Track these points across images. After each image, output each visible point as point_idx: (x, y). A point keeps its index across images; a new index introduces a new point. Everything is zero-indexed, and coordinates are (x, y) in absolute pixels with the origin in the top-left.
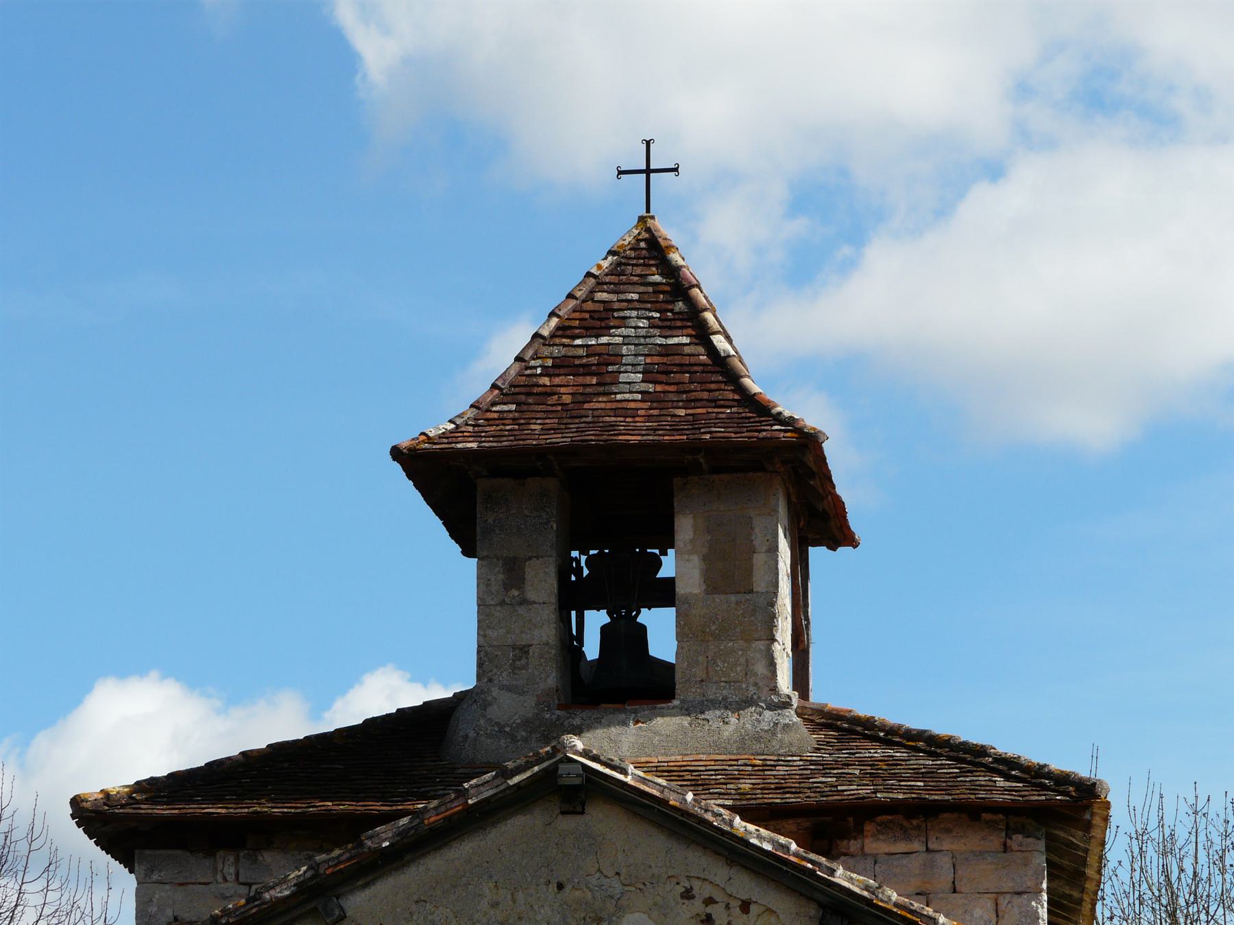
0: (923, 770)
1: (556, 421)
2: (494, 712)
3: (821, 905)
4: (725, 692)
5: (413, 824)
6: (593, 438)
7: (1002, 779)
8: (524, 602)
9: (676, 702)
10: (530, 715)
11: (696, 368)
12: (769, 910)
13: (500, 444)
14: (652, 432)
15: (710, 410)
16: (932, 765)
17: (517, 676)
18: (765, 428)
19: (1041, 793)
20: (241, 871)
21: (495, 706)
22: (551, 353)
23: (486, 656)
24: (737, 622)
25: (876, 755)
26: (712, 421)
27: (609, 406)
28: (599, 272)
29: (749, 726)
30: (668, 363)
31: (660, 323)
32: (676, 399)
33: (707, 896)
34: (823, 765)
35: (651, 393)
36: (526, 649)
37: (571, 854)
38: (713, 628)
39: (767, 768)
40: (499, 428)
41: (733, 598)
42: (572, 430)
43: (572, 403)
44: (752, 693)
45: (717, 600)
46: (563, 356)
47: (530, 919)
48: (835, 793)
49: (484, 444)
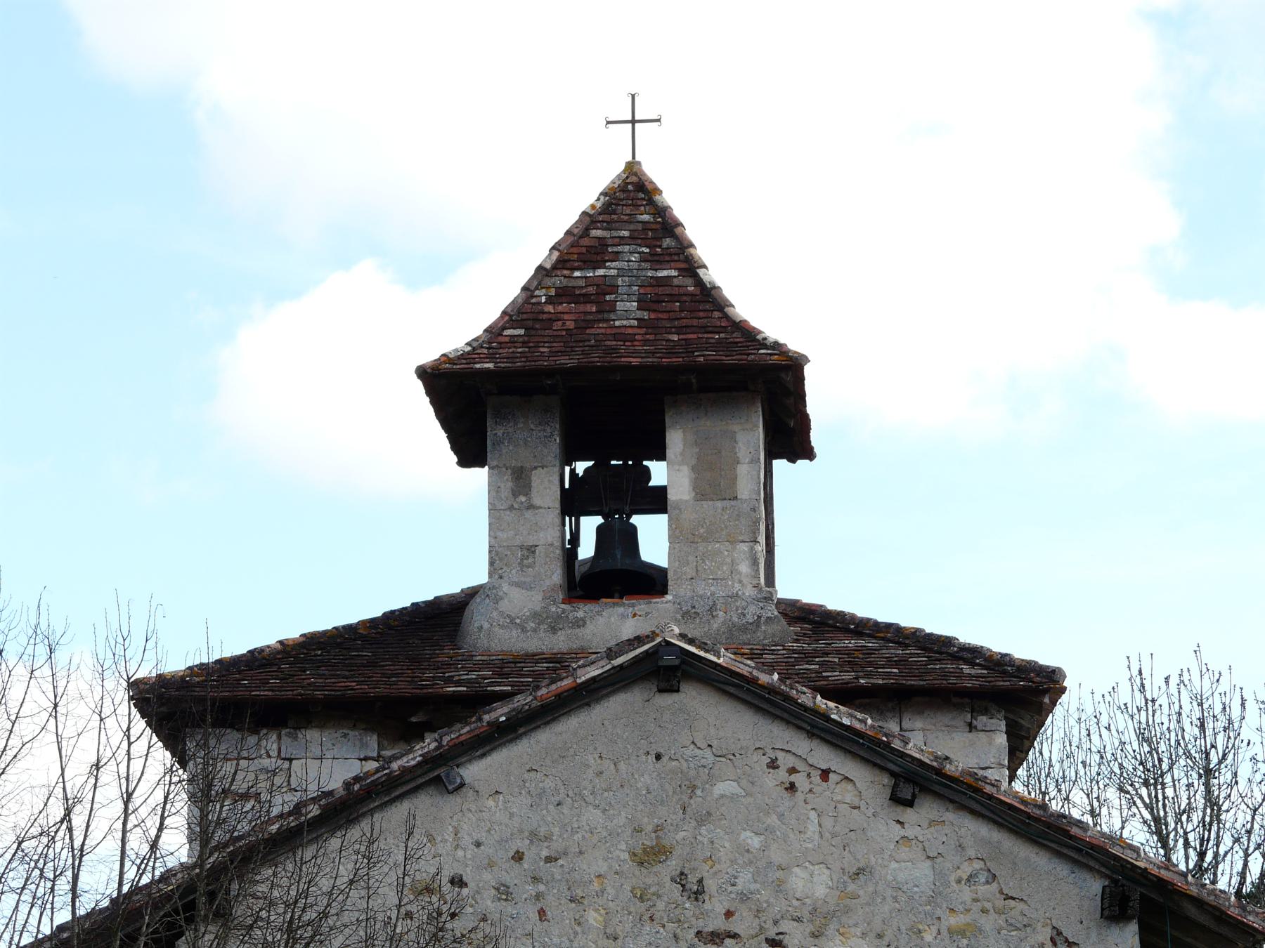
0: (896, 659)
1: (562, 344)
2: (504, 605)
3: (893, 774)
4: (712, 588)
5: (527, 701)
6: (598, 359)
7: (968, 667)
8: (531, 507)
9: (669, 597)
10: (538, 609)
11: (685, 298)
12: (847, 778)
13: (514, 365)
14: (650, 355)
15: (700, 336)
16: (902, 654)
17: (524, 574)
18: (753, 352)
19: (1005, 679)
20: (283, 748)
21: (506, 601)
22: (554, 284)
23: (497, 555)
24: (723, 526)
25: (850, 645)
26: (703, 345)
27: (609, 331)
28: (593, 212)
29: (735, 619)
30: (660, 293)
31: (650, 258)
32: (669, 326)
33: (791, 766)
34: (805, 654)
35: (646, 320)
36: (533, 549)
37: (667, 728)
38: (702, 531)
39: (755, 656)
40: (511, 350)
41: (719, 504)
42: (578, 352)
43: (575, 328)
44: (737, 589)
45: (705, 506)
46: (564, 287)
47: (631, 786)
48: (821, 679)
49: (499, 365)
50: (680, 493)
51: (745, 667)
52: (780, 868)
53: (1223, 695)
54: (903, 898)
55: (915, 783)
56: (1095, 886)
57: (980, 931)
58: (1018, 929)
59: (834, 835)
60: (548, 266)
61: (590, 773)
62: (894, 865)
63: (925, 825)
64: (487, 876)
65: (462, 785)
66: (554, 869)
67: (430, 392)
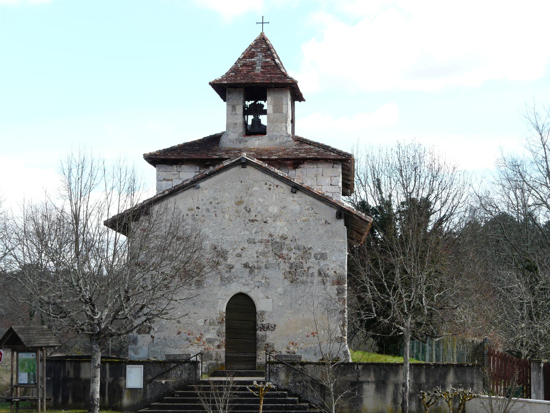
2: (229, 137)
3: (292, 186)
8: (236, 114)
9: (267, 135)
10: (237, 138)
29: (281, 141)
41: (279, 114)
50: (270, 111)
51: (260, 163)
52: (267, 206)
53: (434, 146)
54: (293, 213)
55: (296, 188)
56: (335, 211)
57: (310, 220)
58: (318, 220)
59: (279, 199)
60: (241, 58)
61: (227, 185)
62: (291, 206)
63: (299, 197)
64: (204, 207)
65: (199, 187)
66: (219, 206)
67: (213, 87)
